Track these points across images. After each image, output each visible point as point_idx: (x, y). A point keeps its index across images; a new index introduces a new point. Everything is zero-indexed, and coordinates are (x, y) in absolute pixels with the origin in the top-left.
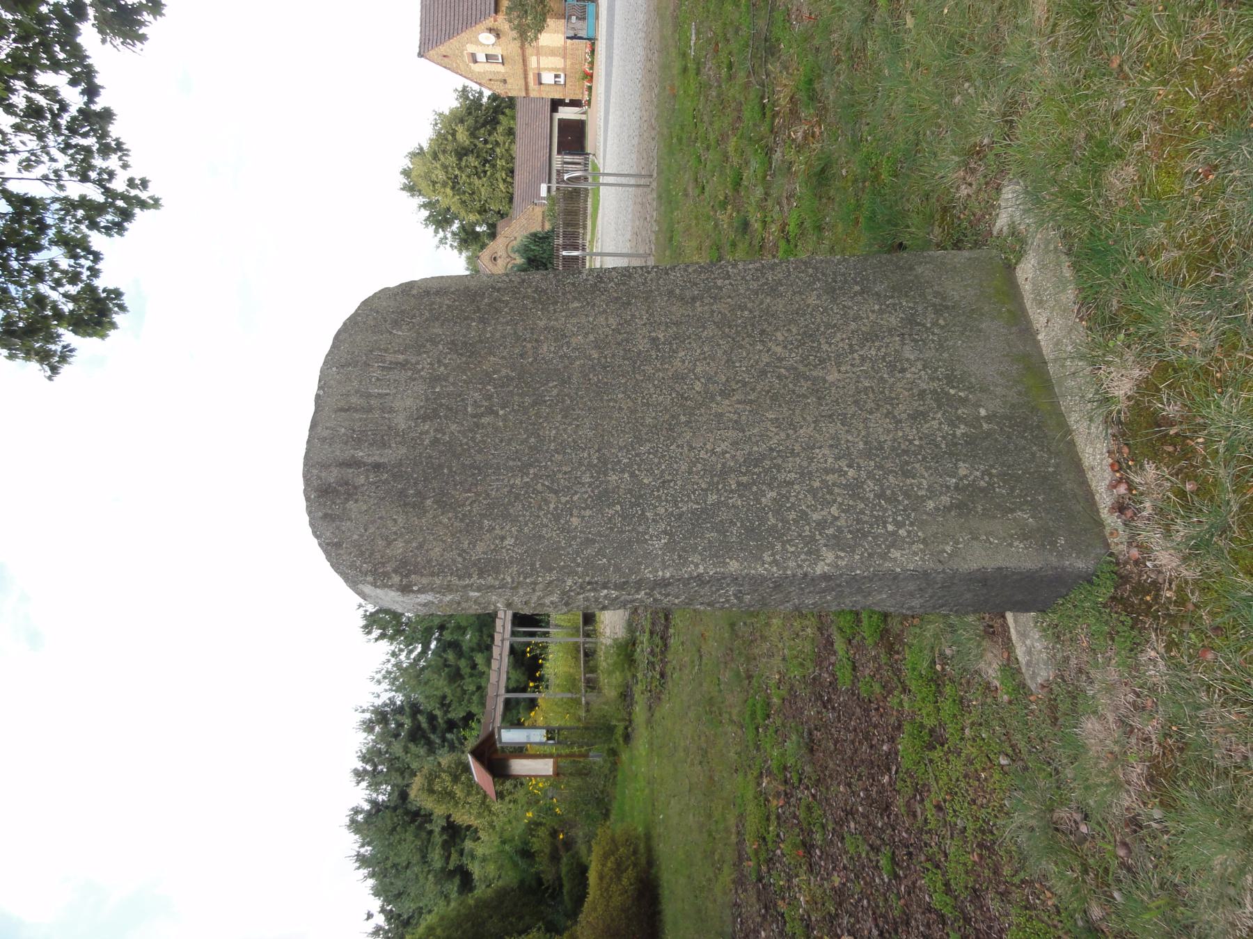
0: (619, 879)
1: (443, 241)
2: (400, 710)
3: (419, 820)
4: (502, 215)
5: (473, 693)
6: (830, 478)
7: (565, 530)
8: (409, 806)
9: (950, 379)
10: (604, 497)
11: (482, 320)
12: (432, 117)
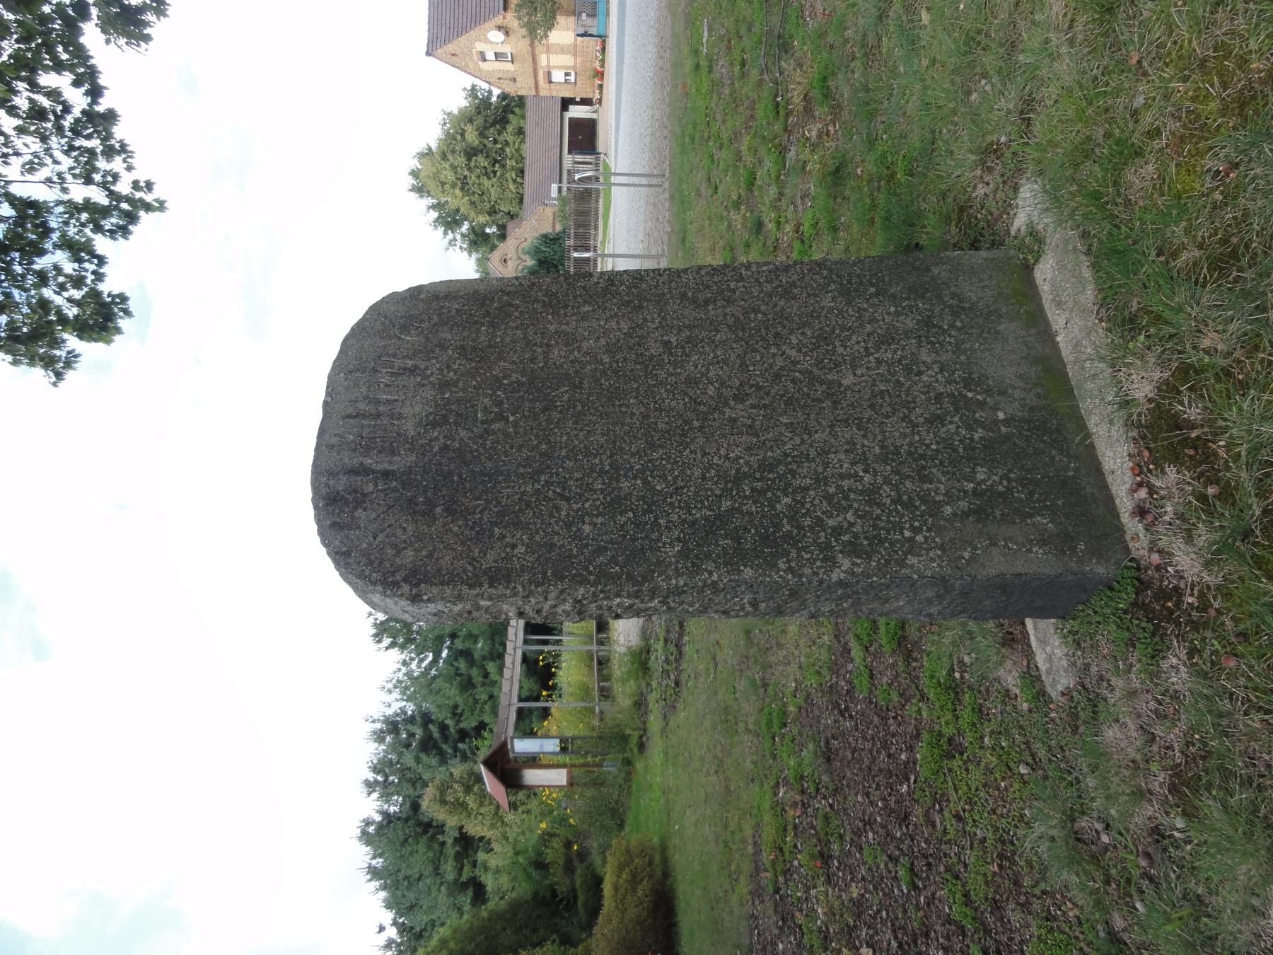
0: (635, 891)
1: (452, 243)
4: (512, 216)
5: (485, 702)
6: (846, 483)
7: (577, 537)
8: (421, 817)
9: (968, 383)
10: (616, 504)
11: (492, 325)
12: (441, 117)
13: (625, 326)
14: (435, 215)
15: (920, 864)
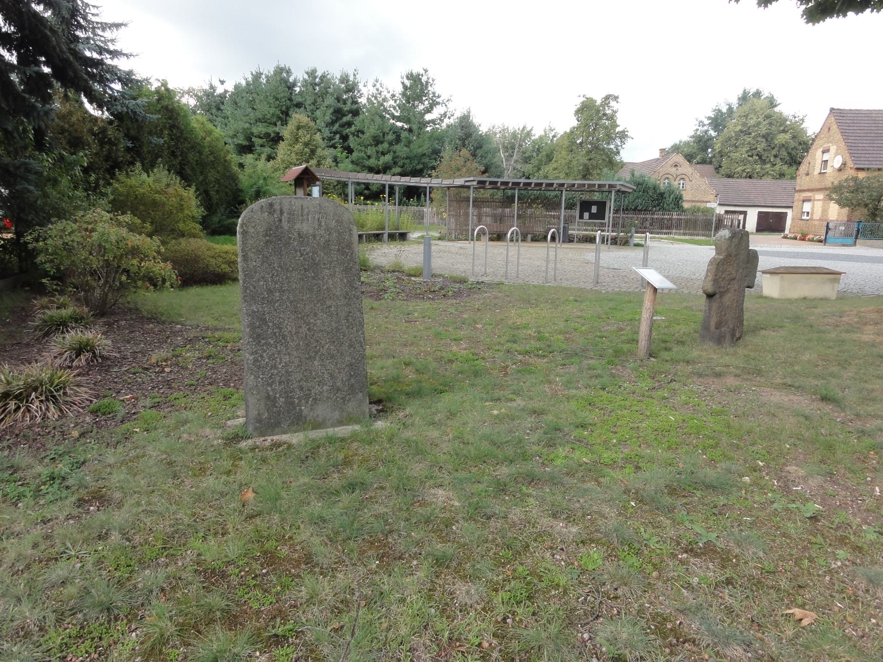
1: (701, 123)
2: (355, 102)
3: (284, 117)
5: (366, 153)
7: (259, 280)
8: (292, 110)
9: (315, 399)
10: (270, 291)
11: (338, 250)
13: (338, 293)
14: (724, 110)
15: (193, 388)
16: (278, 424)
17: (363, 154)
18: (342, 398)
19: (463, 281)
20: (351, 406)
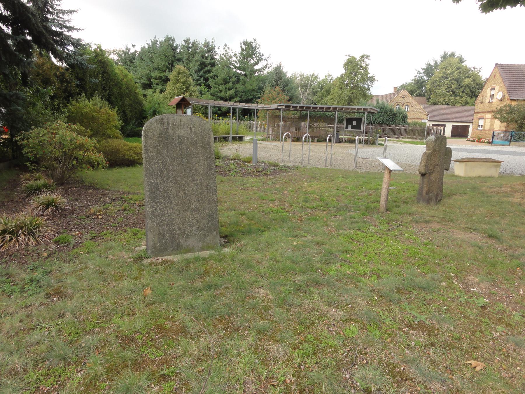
0: (135, 154)
1: (419, 72)
4: (428, 99)
5: (219, 89)
6: (166, 211)
7: (154, 164)
8: (175, 62)
9: (188, 235)
10: (161, 171)
11: (202, 146)
12: (478, 67)
14: (432, 64)
15: (115, 228)
16: (165, 249)
17: (217, 89)
18: (204, 235)
19: (276, 165)
20: (209, 239)
